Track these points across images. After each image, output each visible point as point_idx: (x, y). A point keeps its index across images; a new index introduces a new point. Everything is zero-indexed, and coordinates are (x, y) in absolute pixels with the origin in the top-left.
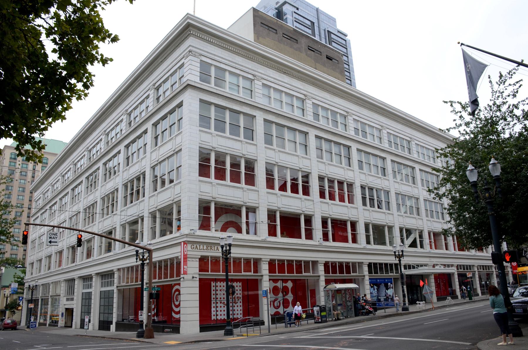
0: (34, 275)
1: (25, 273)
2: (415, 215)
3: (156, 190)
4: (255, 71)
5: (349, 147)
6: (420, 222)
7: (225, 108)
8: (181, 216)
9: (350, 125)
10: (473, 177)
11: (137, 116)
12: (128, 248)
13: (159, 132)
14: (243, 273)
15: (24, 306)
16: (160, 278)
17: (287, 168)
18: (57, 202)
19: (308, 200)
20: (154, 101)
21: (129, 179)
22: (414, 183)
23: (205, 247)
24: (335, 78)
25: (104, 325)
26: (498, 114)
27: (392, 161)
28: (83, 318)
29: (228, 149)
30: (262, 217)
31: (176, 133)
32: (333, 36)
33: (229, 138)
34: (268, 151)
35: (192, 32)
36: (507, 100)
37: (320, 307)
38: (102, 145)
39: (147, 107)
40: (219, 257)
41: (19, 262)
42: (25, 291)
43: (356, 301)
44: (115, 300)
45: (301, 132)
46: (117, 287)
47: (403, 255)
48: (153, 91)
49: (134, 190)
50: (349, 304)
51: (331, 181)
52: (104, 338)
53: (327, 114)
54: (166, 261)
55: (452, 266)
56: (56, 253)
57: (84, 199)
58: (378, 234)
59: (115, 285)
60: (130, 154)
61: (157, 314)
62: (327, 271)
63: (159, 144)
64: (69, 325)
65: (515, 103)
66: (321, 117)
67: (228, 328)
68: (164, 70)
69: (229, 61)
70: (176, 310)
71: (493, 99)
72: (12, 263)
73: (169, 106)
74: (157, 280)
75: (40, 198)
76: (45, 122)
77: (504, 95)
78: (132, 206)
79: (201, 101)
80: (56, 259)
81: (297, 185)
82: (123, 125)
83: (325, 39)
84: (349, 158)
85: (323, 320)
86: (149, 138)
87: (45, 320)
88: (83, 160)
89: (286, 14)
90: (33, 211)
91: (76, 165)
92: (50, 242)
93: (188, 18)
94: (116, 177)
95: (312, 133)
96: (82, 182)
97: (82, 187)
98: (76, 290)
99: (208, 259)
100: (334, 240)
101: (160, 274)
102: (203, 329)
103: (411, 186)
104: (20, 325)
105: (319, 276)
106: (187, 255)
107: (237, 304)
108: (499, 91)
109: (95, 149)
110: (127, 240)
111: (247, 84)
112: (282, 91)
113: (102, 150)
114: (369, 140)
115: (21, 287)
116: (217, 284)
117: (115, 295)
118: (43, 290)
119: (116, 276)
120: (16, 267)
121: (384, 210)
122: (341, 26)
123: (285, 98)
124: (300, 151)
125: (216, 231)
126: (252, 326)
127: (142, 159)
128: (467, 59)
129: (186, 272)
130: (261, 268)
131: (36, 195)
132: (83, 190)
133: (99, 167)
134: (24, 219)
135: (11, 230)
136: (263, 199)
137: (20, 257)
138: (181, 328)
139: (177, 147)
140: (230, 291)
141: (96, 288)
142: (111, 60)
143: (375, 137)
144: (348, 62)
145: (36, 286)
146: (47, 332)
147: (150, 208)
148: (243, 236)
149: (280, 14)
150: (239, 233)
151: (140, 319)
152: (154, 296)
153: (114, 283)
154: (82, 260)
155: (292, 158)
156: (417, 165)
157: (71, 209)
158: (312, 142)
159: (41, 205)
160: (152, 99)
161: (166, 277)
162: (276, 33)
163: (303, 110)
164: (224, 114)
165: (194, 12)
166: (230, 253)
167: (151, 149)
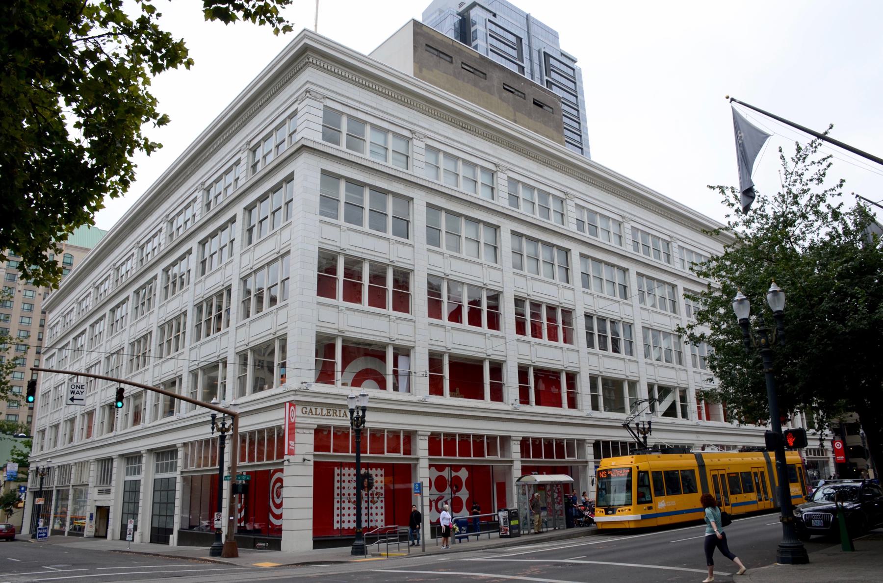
0: (45, 451)
1: (31, 447)
2: (675, 364)
3: (248, 316)
4: (415, 124)
5: (567, 251)
6: (683, 375)
7: (363, 185)
8: (287, 360)
9: (570, 214)
10: (743, 312)
11: (220, 194)
12: (200, 410)
13: (255, 221)
14: (386, 455)
15: (28, 502)
16: (251, 459)
17: (463, 283)
18: (85, 330)
19: (497, 336)
20: (247, 169)
21: (205, 297)
22: (674, 312)
23: (325, 411)
24: (547, 137)
25: (160, 535)
26: (795, 208)
27: (638, 274)
28: (124, 523)
29: (366, 251)
30: (420, 364)
31: (282, 225)
32: (552, 61)
33: (369, 234)
34: (432, 255)
35: (311, 60)
36: (808, 186)
37: (509, 512)
38: (162, 238)
39: (236, 180)
40: (348, 428)
41: (21, 427)
42: (30, 476)
43: (570, 503)
44: (178, 494)
45: (487, 224)
46: (182, 472)
47: (650, 430)
48: (246, 153)
49: (213, 313)
50: (557, 507)
51: (536, 305)
52: (158, 555)
53: (532, 196)
54: (261, 432)
55: (735, 447)
56: (83, 415)
57: (131, 327)
58: (612, 392)
59: (179, 469)
60: (207, 255)
61: (246, 519)
62: (524, 451)
63: (255, 241)
64: (102, 534)
65: (820, 193)
66: (521, 201)
67: (357, 542)
68: (265, 120)
69: (372, 107)
70: (277, 512)
71: (786, 184)
72: (9, 429)
73: (273, 179)
74: (246, 463)
75: (57, 323)
76: (64, 227)
77: (805, 178)
78: (209, 341)
79: (324, 172)
80: (83, 425)
81: (479, 312)
82: (197, 207)
83: (540, 66)
84: (567, 269)
85: (514, 532)
86: (238, 230)
87: (63, 525)
88: (130, 262)
89: (474, 24)
90: (47, 343)
91: (118, 269)
92: (72, 399)
93: (305, 36)
94: (183, 292)
95: (507, 227)
96: (127, 298)
97: (129, 306)
98: (114, 477)
99: (330, 431)
100: (538, 403)
101: (261, 452)
102: (318, 543)
103: (669, 316)
104: (20, 532)
105: (512, 461)
106: (294, 423)
107: (376, 505)
108: (797, 172)
109: (150, 244)
110: (199, 399)
111: (401, 146)
112: (459, 158)
113: (162, 248)
114: (601, 239)
115: (24, 469)
116: (343, 472)
117: (179, 487)
118: (60, 475)
119: (180, 454)
120: (17, 436)
121: (623, 355)
122: (566, 45)
123: (462, 170)
124: (485, 256)
125: (343, 384)
126: (396, 540)
127: (226, 265)
128: (739, 123)
129: (293, 450)
130: (416, 445)
131: (51, 317)
132: (129, 311)
133: (156, 276)
134: (31, 362)
135: (8, 378)
136: (421, 333)
137: (22, 419)
138: (282, 542)
139: (282, 246)
140: (363, 483)
141: (148, 474)
142: (160, 146)
143: (612, 235)
144: (577, 106)
145: (49, 468)
146: (65, 545)
147: (238, 345)
148: (389, 393)
149: (464, 29)
150: (381, 388)
151: (216, 526)
152: (240, 490)
153: (176, 467)
154: (126, 427)
155: (471, 268)
156: (680, 281)
157: (108, 345)
158: (506, 242)
159: (59, 334)
160: (245, 167)
161: (260, 459)
162: (451, 62)
163: (492, 189)
164: (362, 195)
165: (316, 26)
166: (364, 422)
167: (242, 249)
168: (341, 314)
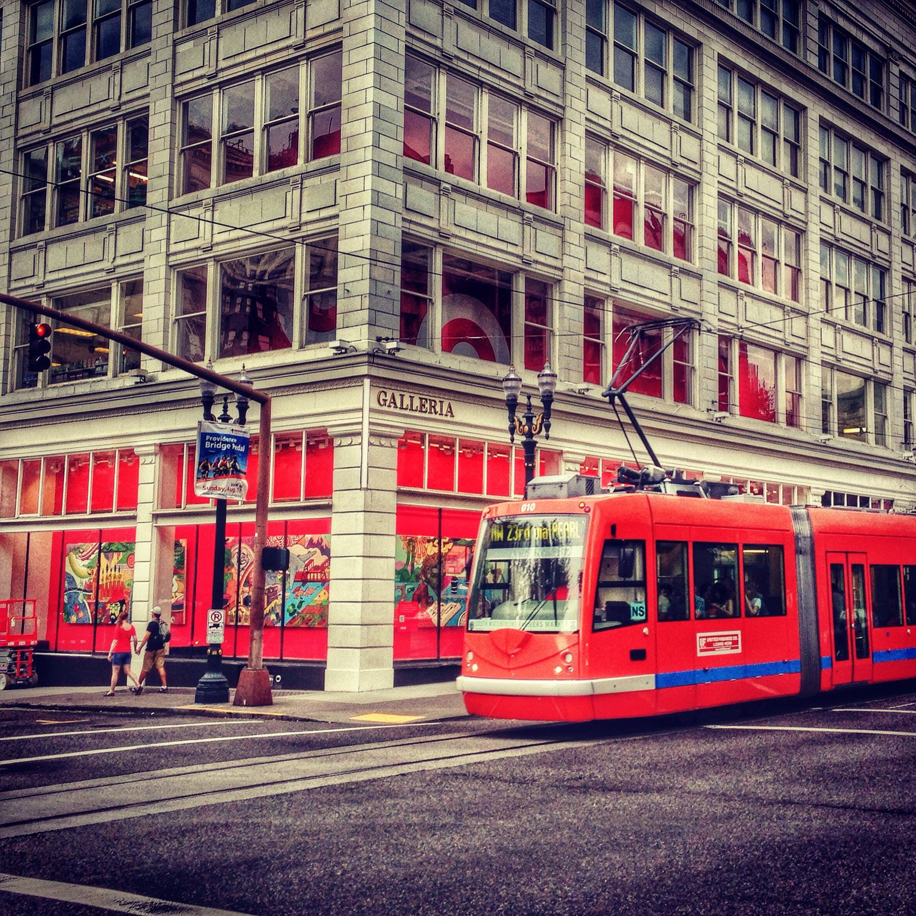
17: (481, 84)
33: (491, 30)
168: (444, 199)
